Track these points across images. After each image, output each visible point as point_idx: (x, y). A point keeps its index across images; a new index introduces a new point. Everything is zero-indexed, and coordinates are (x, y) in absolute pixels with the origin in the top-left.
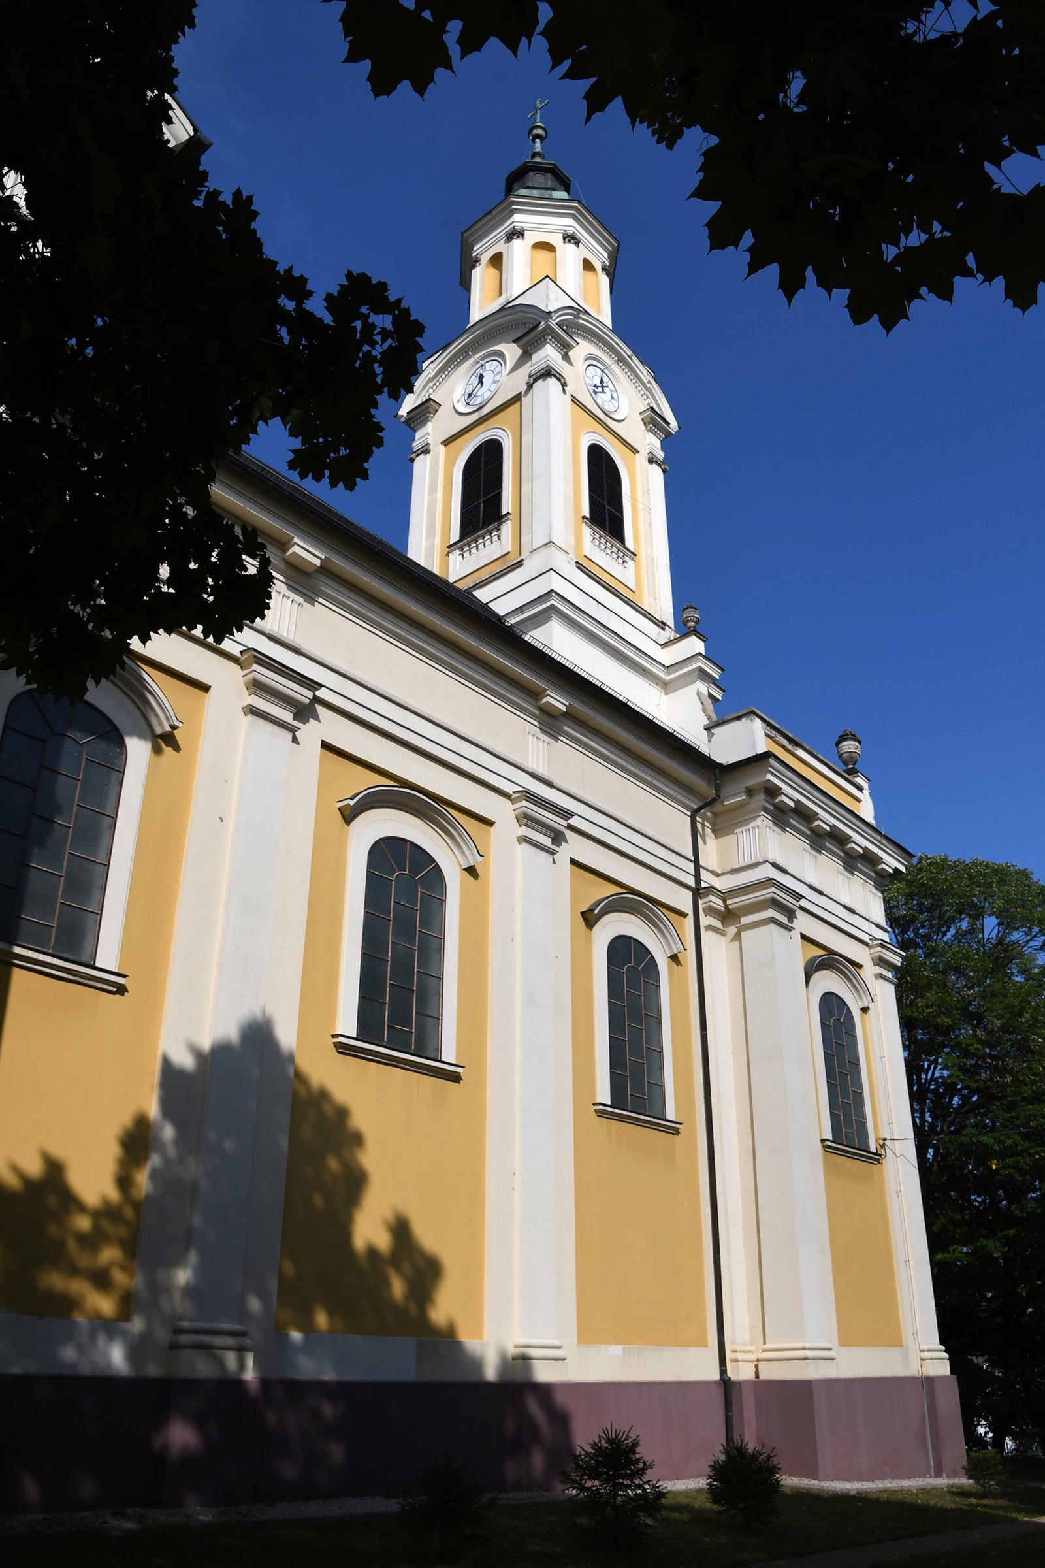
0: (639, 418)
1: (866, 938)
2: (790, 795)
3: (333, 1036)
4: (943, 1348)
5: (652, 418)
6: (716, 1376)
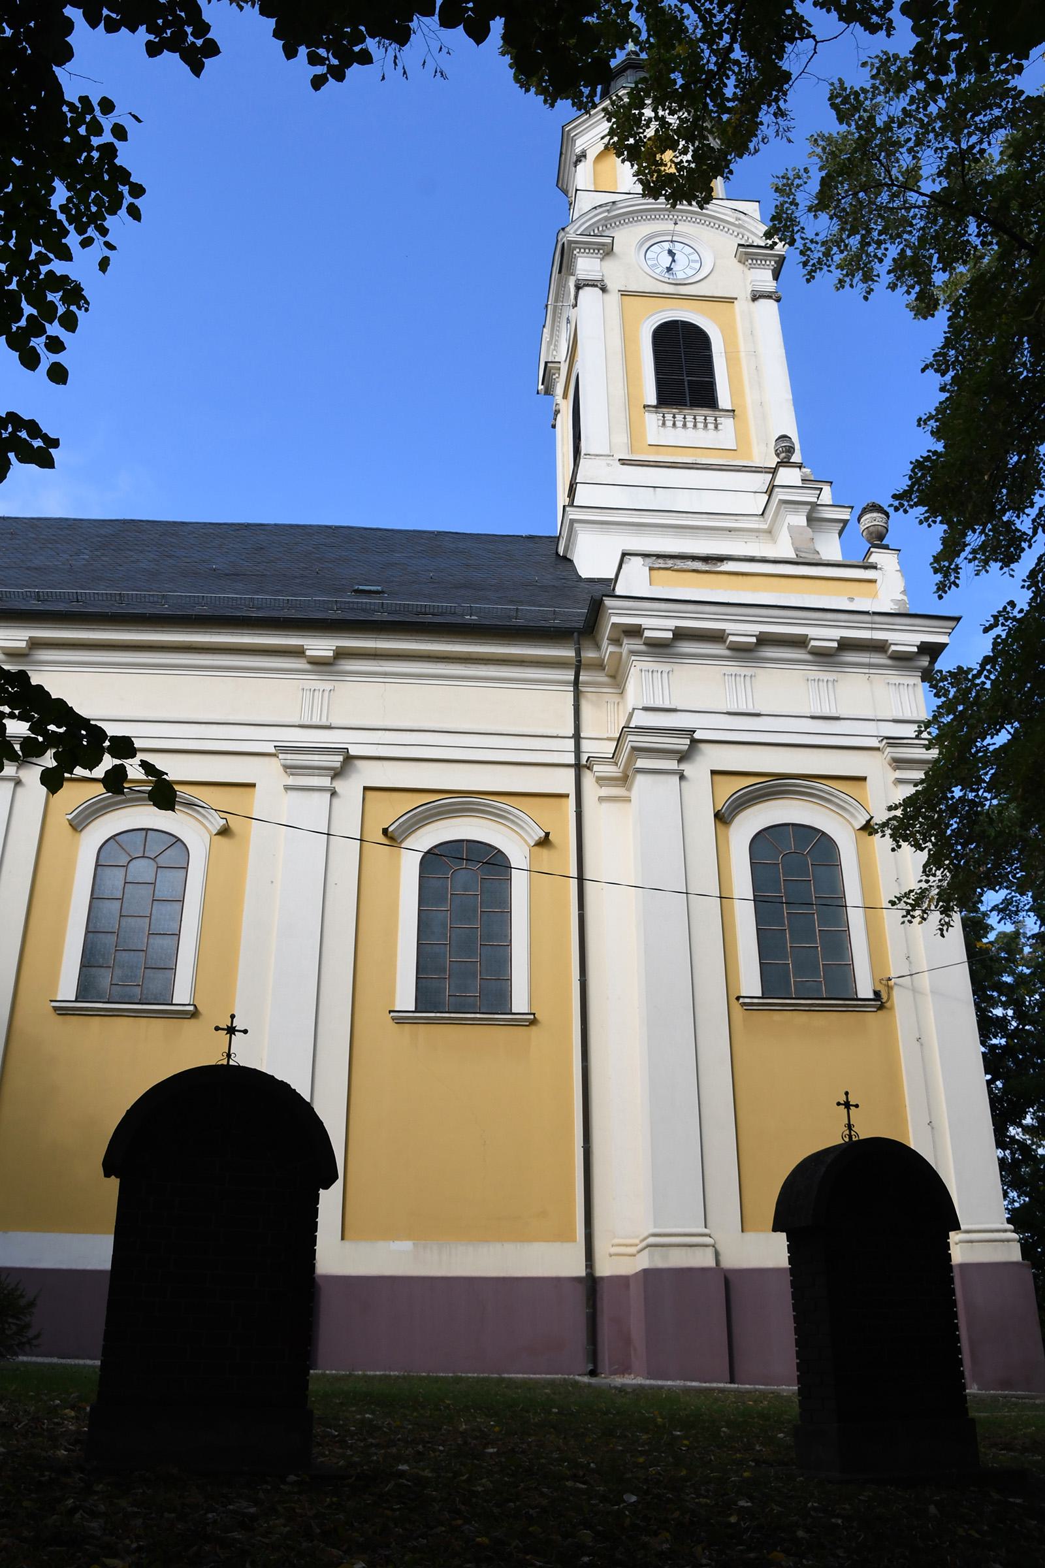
0: (735, 261)
1: (874, 743)
2: (658, 626)
3: (390, 1012)
4: (1011, 1227)
5: (746, 254)
6: (581, 1272)
